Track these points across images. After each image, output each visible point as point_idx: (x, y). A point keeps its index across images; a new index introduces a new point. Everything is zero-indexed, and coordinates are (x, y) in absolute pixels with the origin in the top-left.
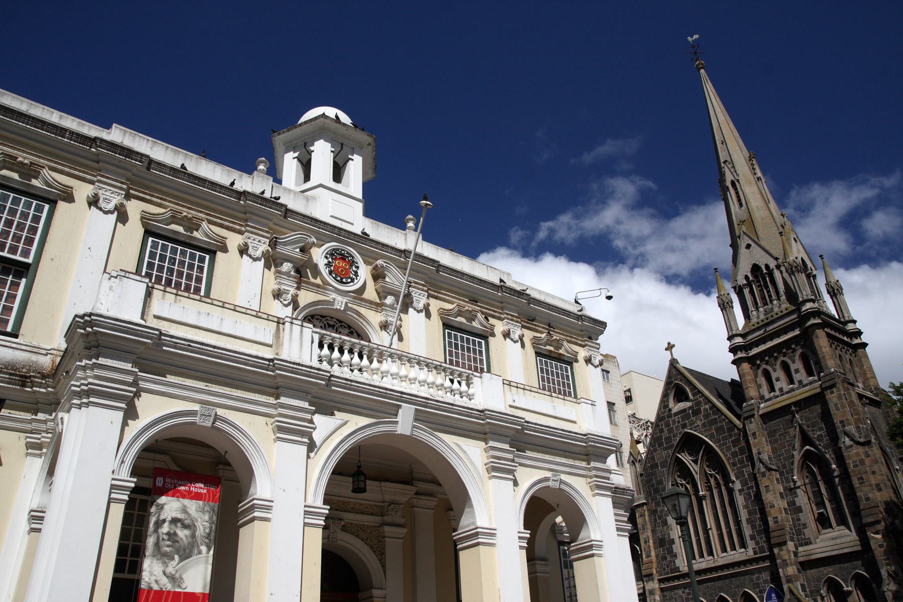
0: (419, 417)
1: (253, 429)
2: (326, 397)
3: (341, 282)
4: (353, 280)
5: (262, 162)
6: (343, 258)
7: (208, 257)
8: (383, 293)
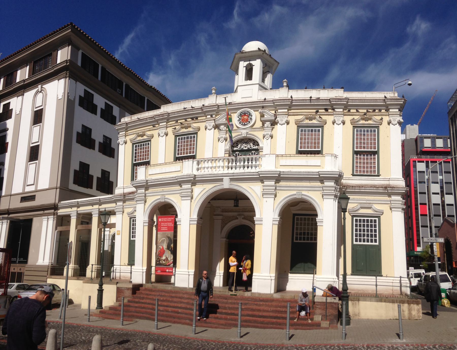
0: (232, 180)
1: (174, 199)
2: (194, 181)
3: (245, 125)
4: (249, 122)
5: (445, 143)
6: (245, 114)
7: (321, 129)
8: (263, 122)
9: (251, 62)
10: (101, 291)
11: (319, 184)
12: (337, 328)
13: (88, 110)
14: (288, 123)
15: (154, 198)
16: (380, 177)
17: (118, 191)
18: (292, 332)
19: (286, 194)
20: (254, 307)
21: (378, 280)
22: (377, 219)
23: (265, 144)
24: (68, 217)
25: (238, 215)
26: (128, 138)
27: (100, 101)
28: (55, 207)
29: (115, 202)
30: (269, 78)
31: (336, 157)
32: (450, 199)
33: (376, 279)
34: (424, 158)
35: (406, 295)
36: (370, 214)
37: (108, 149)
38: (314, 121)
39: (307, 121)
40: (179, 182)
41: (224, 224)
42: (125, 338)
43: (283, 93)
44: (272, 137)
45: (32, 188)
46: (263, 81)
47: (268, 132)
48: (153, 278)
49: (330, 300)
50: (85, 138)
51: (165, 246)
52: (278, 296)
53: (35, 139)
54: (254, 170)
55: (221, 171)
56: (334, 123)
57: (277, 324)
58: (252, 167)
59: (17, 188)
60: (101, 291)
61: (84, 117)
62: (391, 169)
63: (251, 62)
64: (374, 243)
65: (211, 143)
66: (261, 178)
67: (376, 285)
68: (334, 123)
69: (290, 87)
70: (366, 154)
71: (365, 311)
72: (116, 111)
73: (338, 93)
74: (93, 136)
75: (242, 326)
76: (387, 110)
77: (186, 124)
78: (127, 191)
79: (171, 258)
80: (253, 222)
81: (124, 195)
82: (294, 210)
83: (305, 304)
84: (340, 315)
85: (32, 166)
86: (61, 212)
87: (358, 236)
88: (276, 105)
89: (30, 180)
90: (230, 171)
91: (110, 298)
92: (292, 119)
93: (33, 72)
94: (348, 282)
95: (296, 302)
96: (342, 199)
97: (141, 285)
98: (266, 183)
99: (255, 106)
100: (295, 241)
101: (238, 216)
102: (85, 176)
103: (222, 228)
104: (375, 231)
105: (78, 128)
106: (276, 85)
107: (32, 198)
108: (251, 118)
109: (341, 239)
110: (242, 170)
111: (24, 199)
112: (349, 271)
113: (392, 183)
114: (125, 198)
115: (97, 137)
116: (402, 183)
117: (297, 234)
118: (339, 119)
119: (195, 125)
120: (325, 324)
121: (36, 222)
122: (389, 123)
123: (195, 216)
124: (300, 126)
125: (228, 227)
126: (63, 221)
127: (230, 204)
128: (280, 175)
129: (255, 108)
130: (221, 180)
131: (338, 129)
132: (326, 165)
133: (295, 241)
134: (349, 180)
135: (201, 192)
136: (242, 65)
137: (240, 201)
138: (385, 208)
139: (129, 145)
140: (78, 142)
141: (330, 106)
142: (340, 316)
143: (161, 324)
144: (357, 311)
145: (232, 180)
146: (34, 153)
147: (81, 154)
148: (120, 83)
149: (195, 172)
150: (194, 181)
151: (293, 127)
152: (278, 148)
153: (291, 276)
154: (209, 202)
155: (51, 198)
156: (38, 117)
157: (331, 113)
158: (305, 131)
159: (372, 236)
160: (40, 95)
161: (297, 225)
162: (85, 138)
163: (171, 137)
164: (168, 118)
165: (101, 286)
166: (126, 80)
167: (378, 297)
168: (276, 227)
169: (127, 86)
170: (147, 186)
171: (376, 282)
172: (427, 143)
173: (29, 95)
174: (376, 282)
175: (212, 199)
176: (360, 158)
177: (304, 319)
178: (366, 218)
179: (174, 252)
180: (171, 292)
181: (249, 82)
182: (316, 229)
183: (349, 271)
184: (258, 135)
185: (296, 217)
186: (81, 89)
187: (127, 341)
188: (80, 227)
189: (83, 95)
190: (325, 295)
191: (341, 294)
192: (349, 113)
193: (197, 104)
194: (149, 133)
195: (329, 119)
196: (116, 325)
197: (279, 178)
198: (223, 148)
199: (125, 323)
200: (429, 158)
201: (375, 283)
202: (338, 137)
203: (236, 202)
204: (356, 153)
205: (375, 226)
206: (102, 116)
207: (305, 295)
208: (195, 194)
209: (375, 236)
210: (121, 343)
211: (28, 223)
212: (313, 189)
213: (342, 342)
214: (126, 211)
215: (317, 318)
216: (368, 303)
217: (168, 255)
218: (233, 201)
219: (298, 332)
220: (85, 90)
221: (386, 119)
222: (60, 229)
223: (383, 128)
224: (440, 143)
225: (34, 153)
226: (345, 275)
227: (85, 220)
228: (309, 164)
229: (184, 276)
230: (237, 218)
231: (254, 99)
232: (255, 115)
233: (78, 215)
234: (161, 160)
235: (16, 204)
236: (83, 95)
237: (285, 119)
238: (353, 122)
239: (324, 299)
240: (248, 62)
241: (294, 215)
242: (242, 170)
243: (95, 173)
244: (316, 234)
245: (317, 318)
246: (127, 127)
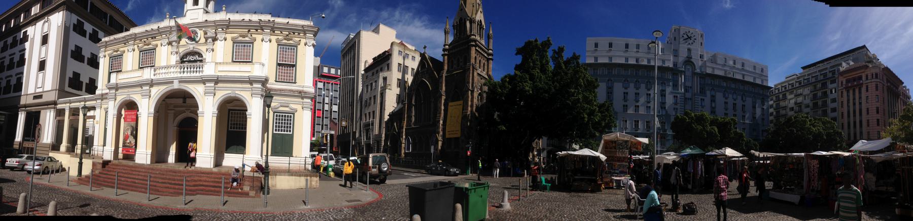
0: (180, 82)
1: (137, 98)
2: (151, 84)
5: (336, 72)
10: (81, 164)
11: (249, 86)
12: (259, 197)
13: (79, 34)
14: (225, 39)
15: (122, 97)
17: (98, 92)
18: (226, 198)
19: (222, 93)
20: (196, 178)
23: (207, 56)
24: (64, 110)
26: (107, 53)
27: (88, 28)
28: (55, 103)
29: (96, 100)
30: (212, 4)
31: (263, 65)
32: (335, 108)
34: (322, 79)
37: (94, 63)
38: (247, 39)
39: (241, 38)
40: (140, 85)
41: (175, 116)
42: (88, 202)
43: (222, 16)
44: (213, 50)
45: (41, 90)
46: (207, 6)
47: (210, 46)
48: (121, 156)
49: (256, 175)
50: (77, 55)
51: (129, 133)
52: (216, 170)
53: (43, 55)
54: (198, 74)
55: (172, 75)
56: (262, 40)
57: (215, 191)
59: (31, 90)
60: (81, 164)
61: (76, 39)
62: (305, 78)
65: (166, 55)
66: (203, 81)
68: (262, 40)
69: (228, 11)
70: (287, 66)
71: (280, 183)
72: (101, 34)
73: (266, 17)
74: (83, 53)
75: (186, 194)
76: (305, 34)
77: (147, 42)
78: (104, 92)
79: (133, 142)
80: (197, 114)
81: (102, 95)
82: (230, 107)
83: (237, 176)
84: (262, 188)
85: (41, 75)
86: (59, 106)
87: (278, 127)
88: (217, 25)
89: (39, 85)
91: (87, 170)
92: (229, 36)
93: (42, 8)
95: (230, 175)
96: (268, 96)
97: (110, 161)
98: (208, 85)
99: (200, 25)
102: (77, 82)
105: (72, 47)
106: (217, 11)
107: (40, 97)
109: (265, 128)
110: (189, 75)
111: (35, 97)
112: (269, 153)
113: (305, 89)
114: (103, 97)
115: (86, 54)
116: (312, 90)
118: (267, 38)
119: (154, 43)
120: (252, 193)
121: (42, 112)
122: (306, 44)
123: (152, 110)
124: (235, 42)
125: (177, 117)
126: (60, 113)
127: (180, 101)
129: (200, 28)
130: (172, 82)
131: (266, 45)
132: (256, 71)
134: (272, 85)
135: (157, 92)
138: (299, 107)
139: (107, 58)
140: (72, 57)
141: (260, 27)
142: (263, 188)
143: (120, 192)
144: (274, 183)
145: (180, 82)
146: (42, 66)
147: (74, 66)
148: (106, 14)
149: (153, 77)
150: (151, 84)
151: (229, 43)
152: (218, 58)
153: (226, 155)
155: (52, 97)
156: (45, 40)
160: (46, 24)
162: (77, 55)
163: (137, 51)
164: (135, 37)
165: (81, 159)
166: (110, 12)
167: (290, 172)
168: (215, 119)
169: (111, 17)
170: (117, 88)
172: (326, 70)
173: (40, 24)
175: (167, 98)
177: (235, 188)
179: (136, 137)
180: (132, 167)
181: (196, 7)
182: (246, 121)
183: (269, 153)
184: (202, 49)
186: (75, 18)
187: (89, 205)
188: (71, 118)
190: (253, 171)
191: (263, 169)
193: (154, 26)
194: (121, 49)
195: (259, 37)
196: (86, 190)
197: (217, 81)
198: (174, 59)
199: (93, 188)
200: (325, 80)
202: (266, 52)
204: (279, 65)
206: (90, 39)
207: (237, 170)
208: (152, 94)
210: (81, 206)
211: (37, 114)
212: (244, 89)
213: (264, 210)
214: (103, 106)
215: (246, 188)
216: (283, 177)
217: (131, 139)
219: (231, 199)
221: (303, 41)
222: (58, 118)
223: (301, 48)
224: (333, 71)
225: (42, 66)
226: (267, 156)
227: (75, 112)
229: (143, 155)
231: (200, 20)
232: (200, 33)
233: (70, 109)
234: (129, 68)
235: (30, 101)
237: (224, 36)
238: (278, 40)
239: (251, 174)
241: (230, 110)
243: (85, 80)
244: (246, 125)
245: (246, 188)
246: (107, 45)
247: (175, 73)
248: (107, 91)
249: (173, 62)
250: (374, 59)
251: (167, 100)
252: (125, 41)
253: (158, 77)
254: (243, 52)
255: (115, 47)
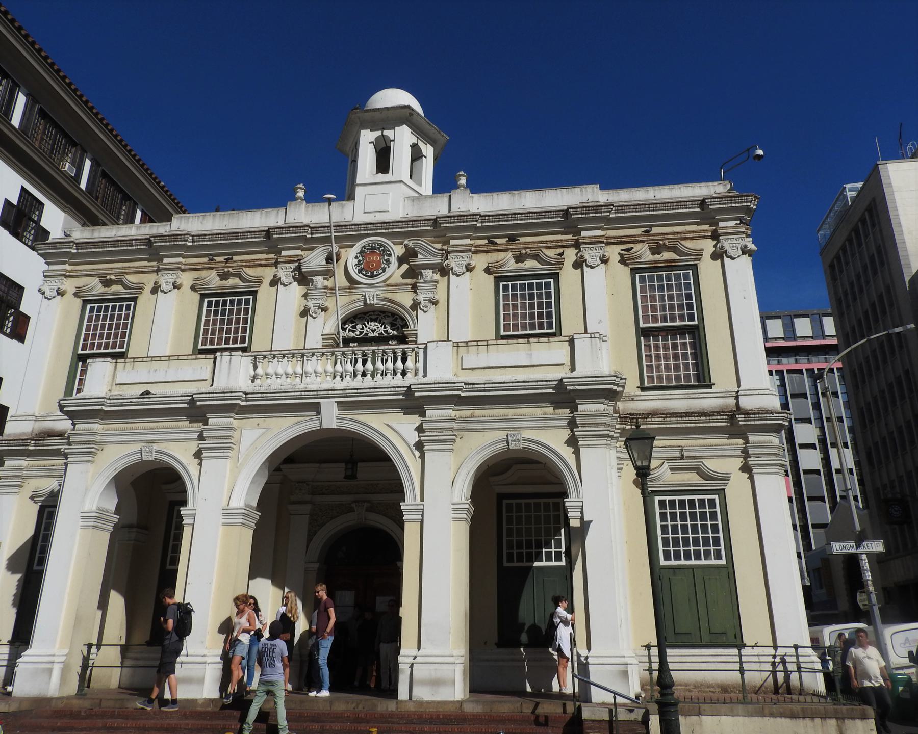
0: (342, 406)
3: (372, 276)
7: (552, 281)
9: (386, 133)
16: (714, 389)
19: (479, 445)
21: (744, 659)
22: (716, 497)
23: (425, 326)
25: (355, 502)
32: (845, 458)
33: (740, 656)
35: (815, 694)
36: (690, 485)
40: (196, 411)
55: (313, 383)
58: (373, 376)
63: (386, 133)
64: (713, 562)
66: (412, 403)
67: (742, 671)
70: (676, 337)
90: (338, 384)
94: (671, 666)
96: (638, 439)
100: (506, 564)
101: (354, 505)
103: (309, 541)
104: (715, 528)
108: (388, 261)
110: (358, 382)
117: (510, 546)
127: (335, 472)
128: (192, 401)
133: (506, 564)
136: (367, 137)
137: (359, 464)
152: (458, 327)
154: (278, 469)
157: (504, 247)
158: (514, 288)
159: (706, 542)
161: (509, 521)
171: (741, 662)
174: (741, 662)
175: (289, 460)
176: (657, 347)
178: (687, 498)
181: (381, 177)
185: (505, 502)
189: (15, 201)
192: (491, 246)
201: (737, 666)
203: (350, 466)
204: (644, 333)
205: (713, 516)
209: (717, 542)
216: (727, 722)
218: (343, 465)
220: (23, 189)
228: (540, 362)
230: (351, 510)
236: (15, 201)
240: (379, 133)
241: (501, 497)
242: (358, 382)
247: (319, 375)
248: (65, 424)
249: (315, 341)
250: (14, 605)
251: (295, 472)
252: (152, 250)
253: (263, 385)
254: (530, 307)
255: (112, 268)
